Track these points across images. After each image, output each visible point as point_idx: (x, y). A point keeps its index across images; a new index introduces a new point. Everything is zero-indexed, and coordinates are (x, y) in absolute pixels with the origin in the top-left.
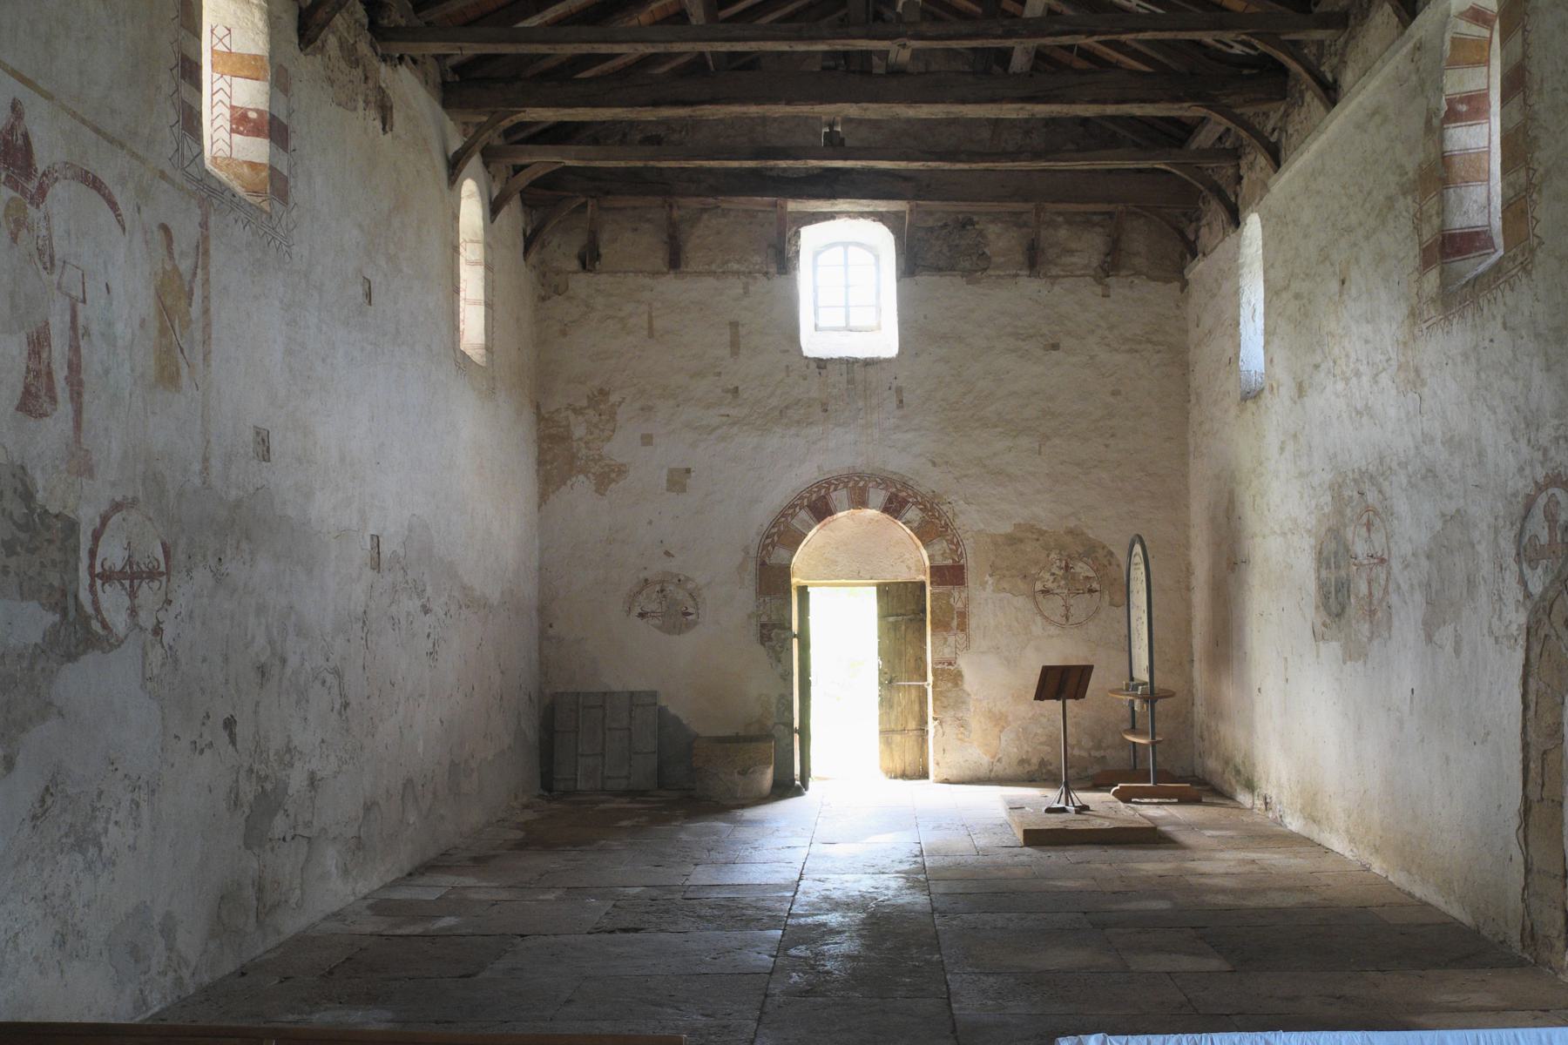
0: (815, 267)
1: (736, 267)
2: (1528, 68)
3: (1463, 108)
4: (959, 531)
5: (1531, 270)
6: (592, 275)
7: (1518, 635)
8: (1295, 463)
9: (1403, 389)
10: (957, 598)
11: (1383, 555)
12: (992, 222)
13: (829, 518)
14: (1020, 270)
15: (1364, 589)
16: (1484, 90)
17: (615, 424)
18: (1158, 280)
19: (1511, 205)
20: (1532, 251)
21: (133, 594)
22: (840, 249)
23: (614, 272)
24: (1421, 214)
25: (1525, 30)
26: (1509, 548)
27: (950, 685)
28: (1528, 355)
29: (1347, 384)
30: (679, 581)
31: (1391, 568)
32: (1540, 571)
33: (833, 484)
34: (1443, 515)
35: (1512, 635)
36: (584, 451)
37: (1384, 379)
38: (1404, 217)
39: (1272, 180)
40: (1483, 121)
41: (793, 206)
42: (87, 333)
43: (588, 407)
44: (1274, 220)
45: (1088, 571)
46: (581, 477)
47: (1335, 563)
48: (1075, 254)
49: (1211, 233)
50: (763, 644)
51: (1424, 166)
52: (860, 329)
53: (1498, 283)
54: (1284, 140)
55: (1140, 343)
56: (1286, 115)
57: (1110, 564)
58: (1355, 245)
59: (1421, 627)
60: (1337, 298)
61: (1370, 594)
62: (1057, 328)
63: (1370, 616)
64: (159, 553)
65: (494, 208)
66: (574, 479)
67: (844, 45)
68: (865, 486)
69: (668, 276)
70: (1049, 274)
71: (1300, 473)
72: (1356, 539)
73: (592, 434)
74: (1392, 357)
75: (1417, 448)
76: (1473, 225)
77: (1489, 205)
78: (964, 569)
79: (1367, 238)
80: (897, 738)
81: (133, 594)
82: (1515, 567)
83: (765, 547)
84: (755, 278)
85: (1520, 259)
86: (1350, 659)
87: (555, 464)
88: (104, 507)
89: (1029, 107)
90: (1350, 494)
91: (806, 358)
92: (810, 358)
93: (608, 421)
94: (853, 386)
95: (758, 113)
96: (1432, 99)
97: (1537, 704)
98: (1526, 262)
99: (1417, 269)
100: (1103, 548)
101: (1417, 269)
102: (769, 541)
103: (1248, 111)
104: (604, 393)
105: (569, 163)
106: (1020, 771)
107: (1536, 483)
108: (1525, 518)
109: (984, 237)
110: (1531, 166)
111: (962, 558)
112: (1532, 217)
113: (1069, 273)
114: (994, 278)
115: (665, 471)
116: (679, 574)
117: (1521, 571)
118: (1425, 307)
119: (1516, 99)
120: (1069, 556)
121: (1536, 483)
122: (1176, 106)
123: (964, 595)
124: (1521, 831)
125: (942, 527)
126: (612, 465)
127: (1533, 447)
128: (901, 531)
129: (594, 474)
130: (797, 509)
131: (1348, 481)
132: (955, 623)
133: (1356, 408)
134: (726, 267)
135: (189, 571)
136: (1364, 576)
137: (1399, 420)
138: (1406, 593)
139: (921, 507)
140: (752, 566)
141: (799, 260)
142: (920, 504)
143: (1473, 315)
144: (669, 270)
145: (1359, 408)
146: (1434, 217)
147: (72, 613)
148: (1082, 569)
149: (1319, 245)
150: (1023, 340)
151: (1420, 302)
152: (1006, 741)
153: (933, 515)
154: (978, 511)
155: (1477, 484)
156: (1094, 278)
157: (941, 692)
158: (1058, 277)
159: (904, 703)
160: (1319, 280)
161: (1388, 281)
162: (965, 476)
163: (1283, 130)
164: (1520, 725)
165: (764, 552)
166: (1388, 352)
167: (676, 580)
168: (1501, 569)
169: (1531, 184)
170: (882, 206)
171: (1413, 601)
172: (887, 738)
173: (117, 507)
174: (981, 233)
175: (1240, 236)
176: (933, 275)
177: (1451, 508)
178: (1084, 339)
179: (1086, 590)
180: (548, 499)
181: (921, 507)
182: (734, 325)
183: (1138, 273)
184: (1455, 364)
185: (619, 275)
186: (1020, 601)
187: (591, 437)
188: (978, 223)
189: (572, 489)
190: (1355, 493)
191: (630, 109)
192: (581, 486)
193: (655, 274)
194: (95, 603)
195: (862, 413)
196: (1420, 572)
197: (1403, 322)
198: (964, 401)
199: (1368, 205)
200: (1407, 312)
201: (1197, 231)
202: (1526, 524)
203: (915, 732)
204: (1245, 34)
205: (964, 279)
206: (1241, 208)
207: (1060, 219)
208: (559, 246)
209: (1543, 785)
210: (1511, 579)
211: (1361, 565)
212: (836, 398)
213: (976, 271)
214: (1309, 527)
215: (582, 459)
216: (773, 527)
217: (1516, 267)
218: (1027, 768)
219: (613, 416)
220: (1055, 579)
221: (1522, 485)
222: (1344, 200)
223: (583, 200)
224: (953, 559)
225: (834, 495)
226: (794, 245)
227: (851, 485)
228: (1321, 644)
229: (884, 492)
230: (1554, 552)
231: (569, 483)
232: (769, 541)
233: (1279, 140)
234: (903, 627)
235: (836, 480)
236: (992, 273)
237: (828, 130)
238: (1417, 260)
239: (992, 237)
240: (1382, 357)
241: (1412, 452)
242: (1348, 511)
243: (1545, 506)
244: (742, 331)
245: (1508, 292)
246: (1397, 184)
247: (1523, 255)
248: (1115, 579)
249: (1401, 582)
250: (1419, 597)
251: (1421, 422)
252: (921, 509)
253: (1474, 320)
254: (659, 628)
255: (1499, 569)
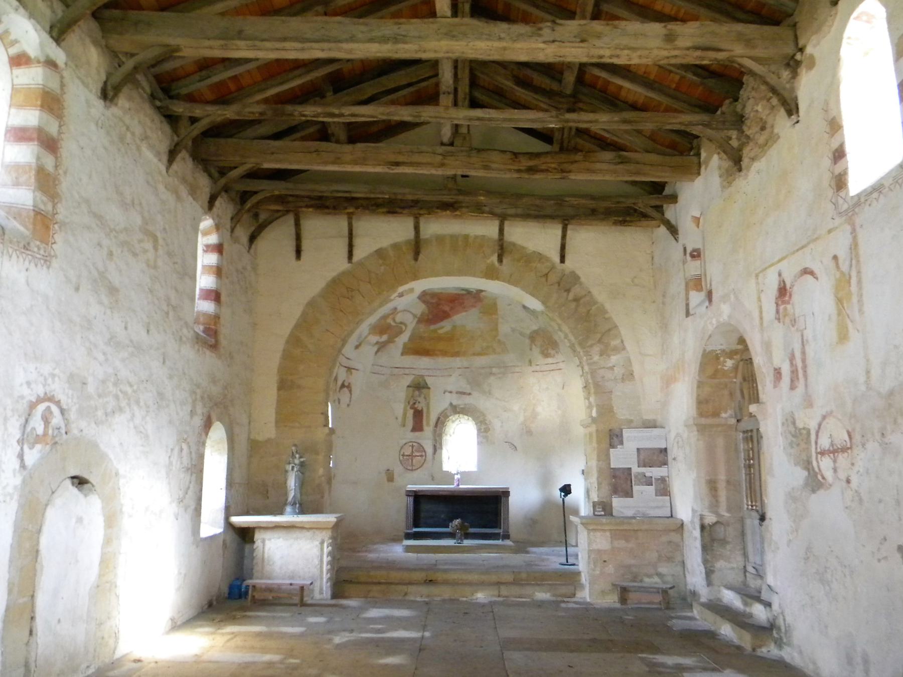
21: (835, 461)
42: (807, 341)
64: (846, 438)
81: (835, 461)
88: (819, 419)
135: (863, 445)
147: (811, 472)
173: (824, 417)
194: (819, 467)
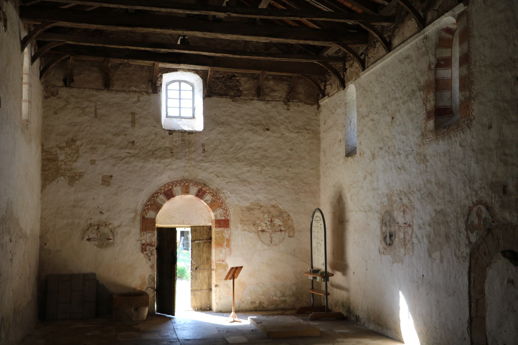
0: (167, 90)
1: (134, 89)
2: (470, 56)
3: (443, 63)
4: (227, 205)
5: (471, 127)
6: (69, 88)
7: (466, 257)
8: (371, 184)
9: (419, 162)
10: (226, 233)
11: (410, 223)
12: (243, 77)
13: (172, 198)
14: (254, 97)
15: (402, 235)
16: (450, 57)
17: (79, 155)
18: (309, 104)
19: (463, 103)
20: (471, 120)
22: (178, 83)
23: (79, 88)
24: (426, 99)
25: (469, 42)
26: (463, 226)
27: (223, 270)
28: (470, 157)
29: (394, 157)
30: (106, 224)
31: (413, 228)
32: (475, 234)
33: (175, 184)
34: (436, 211)
35: (464, 256)
36: (64, 166)
37: (411, 157)
38: (419, 99)
39: (361, 73)
40: (449, 68)
41: (161, 65)
43: (66, 147)
44: (362, 89)
45: (280, 222)
46: (62, 178)
47: (389, 225)
48: (276, 92)
49: (332, 88)
50: (142, 252)
51: (428, 82)
52: (185, 118)
53: (458, 129)
54: (367, 59)
55: (301, 129)
56: (367, 49)
57: (289, 220)
58: (398, 105)
59: (427, 251)
60: (390, 124)
61: (405, 238)
62: (268, 122)
63: (404, 246)
65: (33, 60)
66: (58, 179)
67: (205, 13)
68: (188, 185)
69: (104, 91)
70: (266, 99)
71: (373, 188)
72: (398, 216)
73: (67, 159)
74: (414, 149)
75: (424, 184)
76: (446, 105)
77: (452, 98)
78: (229, 221)
79: (404, 103)
80: (199, 293)
82: (465, 232)
83: (144, 210)
84: (143, 94)
85: (466, 122)
86: (396, 262)
87: (50, 171)
89: (270, 39)
90: (396, 199)
91: (164, 129)
92: (166, 130)
93: (75, 153)
94: (184, 142)
95: (160, 32)
96: (431, 58)
97: (474, 282)
98: (469, 124)
99: (425, 119)
100: (286, 213)
101: (425, 119)
102: (146, 208)
103: (354, 47)
104: (73, 141)
105: (68, 42)
106: (252, 307)
107: (473, 203)
108: (469, 215)
109: (239, 83)
110: (471, 90)
111: (229, 216)
112: (471, 109)
113: (273, 100)
114: (243, 100)
115: (101, 176)
116: (106, 222)
117: (467, 233)
118: (428, 133)
119: (465, 66)
120: (272, 216)
121: (473, 203)
122: (327, 43)
123: (229, 232)
124: (469, 328)
125: (221, 203)
126: (77, 173)
127: (472, 190)
128: (202, 204)
129: (68, 176)
130: (159, 194)
131: (395, 194)
132: (225, 244)
133: (398, 166)
134: (130, 89)
136: (402, 230)
137: (417, 173)
138: (420, 238)
139: (212, 194)
140: (139, 218)
141: (161, 88)
142: (212, 193)
143: (448, 139)
144: (105, 89)
145: (399, 167)
146: (432, 101)
148: (277, 222)
149: (382, 102)
150: (255, 126)
151: (426, 131)
152: (246, 294)
153: (217, 198)
154: (236, 197)
155: (449, 200)
156: (284, 102)
157: (219, 273)
158: (269, 101)
159: (201, 278)
160: (382, 115)
161: (412, 121)
162: (230, 182)
163: (366, 55)
164: (467, 290)
165: (144, 213)
166: (412, 147)
167: (104, 224)
168: (459, 232)
169: (471, 97)
170: (198, 68)
171: (423, 242)
172: (194, 293)
174: (238, 81)
175: (345, 92)
176: (218, 97)
177: (439, 208)
178: (279, 126)
179: (279, 230)
180: (46, 187)
181: (212, 194)
182: (133, 114)
183: (301, 101)
184: (440, 156)
185: (82, 89)
186: (252, 235)
187: (67, 160)
188: (237, 77)
189: (58, 183)
190: (398, 199)
191: (106, 26)
192: (62, 181)
193: (98, 90)
195: (187, 154)
196: (426, 231)
197: (419, 137)
198: (230, 151)
199: (404, 91)
200: (420, 134)
201: (325, 85)
202: (469, 217)
203: (206, 290)
204: (358, 22)
205: (231, 99)
206: (346, 81)
207: (270, 77)
208: (54, 75)
209: (477, 311)
210: (463, 236)
211: (401, 226)
212: (176, 147)
213: (236, 97)
214: (377, 210)
215: (63, 169)
216: (148, 202)
217: (465, 125)
218: (254, 305)
219: (77, 151)
220: (266, 226)
221: (468, 203)
222: (394, 87)
223: (68, 56)
224: (225, 217)
225: (175, 189)
226: (160, 81)
227: (182, 184)
228: (383, 255)
229: (196, 188)
230: (480, 228)
231: (56, 180)
232: (146, 208)
233: (365, 58)
234: (202, 245)
235: (176, 182)
236: (242, 98)
237: (182, 38)
238: (425, 115)
239: (242, 83)
240: (410, 149)
241: (422, 186)
242: (395, 205)
243: (476, 211)
244: (137, 116)
245: (461, 133)
246: (417, 86)
247: (468, 121)
248: (291, 226)
249: (418, 234)
250: (426, 240)
251: (427, 175)
252: (211, 195)
253: (448, 141)
254: (97, 246)
255: (458, 232)
